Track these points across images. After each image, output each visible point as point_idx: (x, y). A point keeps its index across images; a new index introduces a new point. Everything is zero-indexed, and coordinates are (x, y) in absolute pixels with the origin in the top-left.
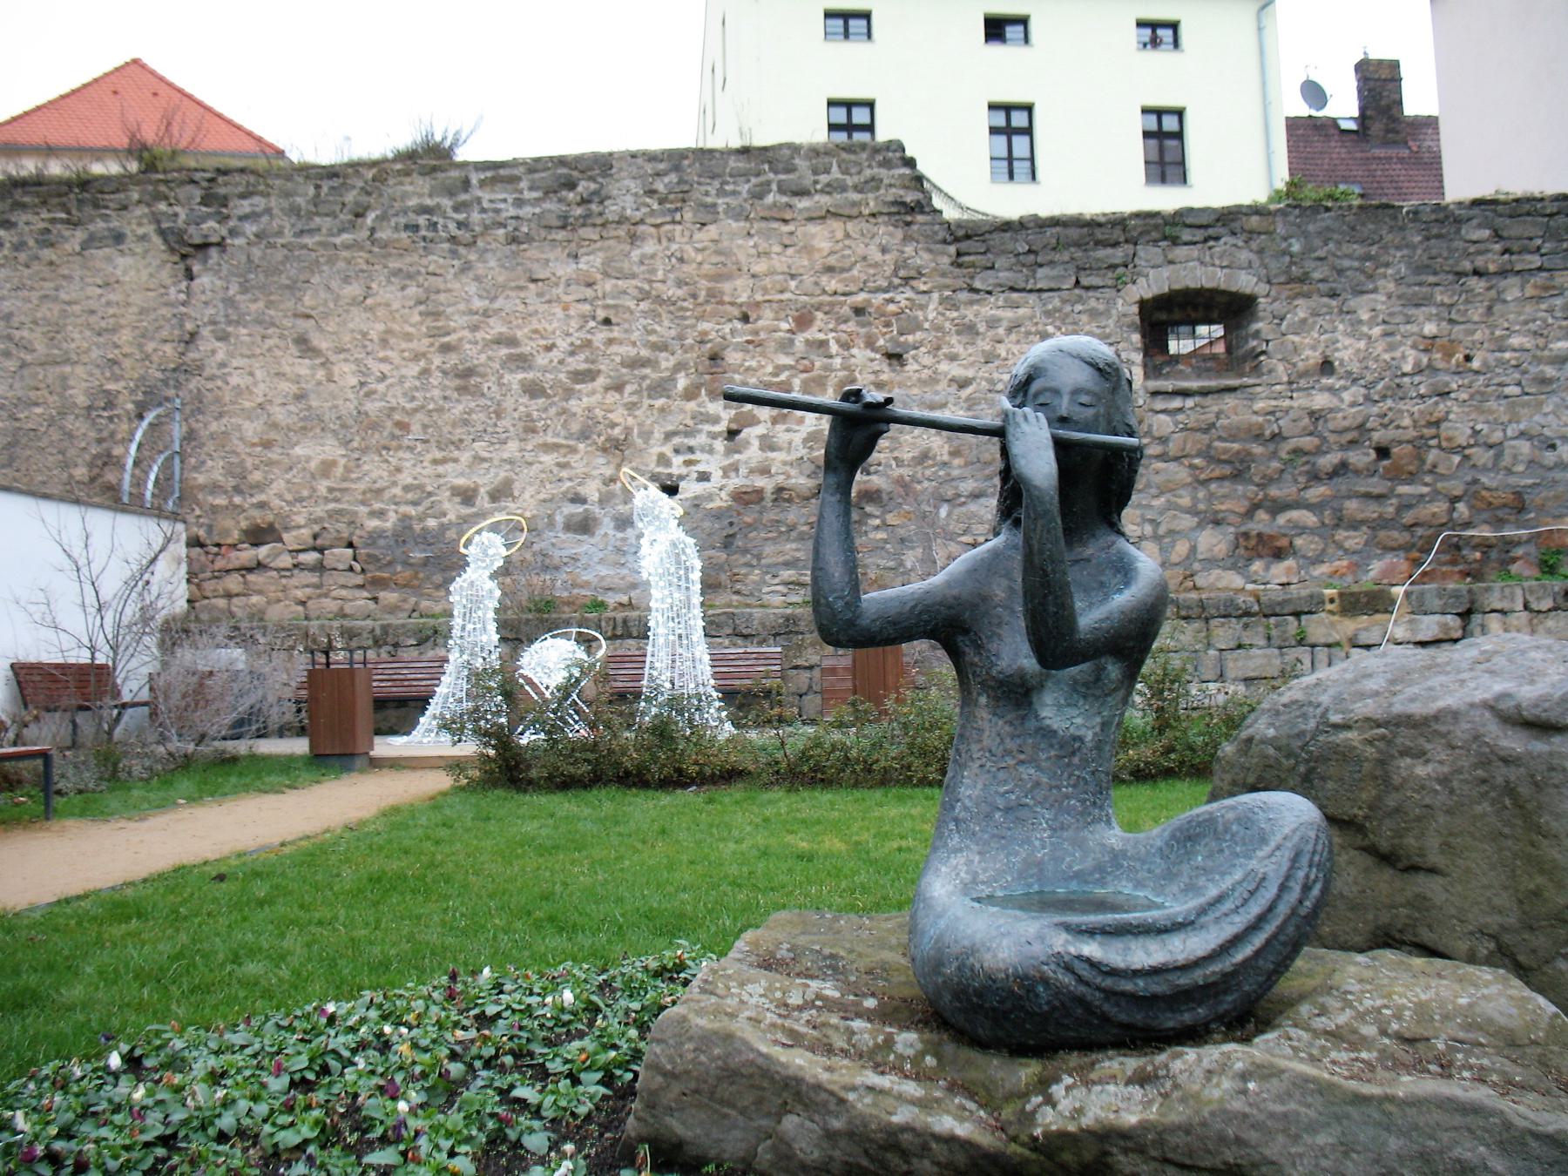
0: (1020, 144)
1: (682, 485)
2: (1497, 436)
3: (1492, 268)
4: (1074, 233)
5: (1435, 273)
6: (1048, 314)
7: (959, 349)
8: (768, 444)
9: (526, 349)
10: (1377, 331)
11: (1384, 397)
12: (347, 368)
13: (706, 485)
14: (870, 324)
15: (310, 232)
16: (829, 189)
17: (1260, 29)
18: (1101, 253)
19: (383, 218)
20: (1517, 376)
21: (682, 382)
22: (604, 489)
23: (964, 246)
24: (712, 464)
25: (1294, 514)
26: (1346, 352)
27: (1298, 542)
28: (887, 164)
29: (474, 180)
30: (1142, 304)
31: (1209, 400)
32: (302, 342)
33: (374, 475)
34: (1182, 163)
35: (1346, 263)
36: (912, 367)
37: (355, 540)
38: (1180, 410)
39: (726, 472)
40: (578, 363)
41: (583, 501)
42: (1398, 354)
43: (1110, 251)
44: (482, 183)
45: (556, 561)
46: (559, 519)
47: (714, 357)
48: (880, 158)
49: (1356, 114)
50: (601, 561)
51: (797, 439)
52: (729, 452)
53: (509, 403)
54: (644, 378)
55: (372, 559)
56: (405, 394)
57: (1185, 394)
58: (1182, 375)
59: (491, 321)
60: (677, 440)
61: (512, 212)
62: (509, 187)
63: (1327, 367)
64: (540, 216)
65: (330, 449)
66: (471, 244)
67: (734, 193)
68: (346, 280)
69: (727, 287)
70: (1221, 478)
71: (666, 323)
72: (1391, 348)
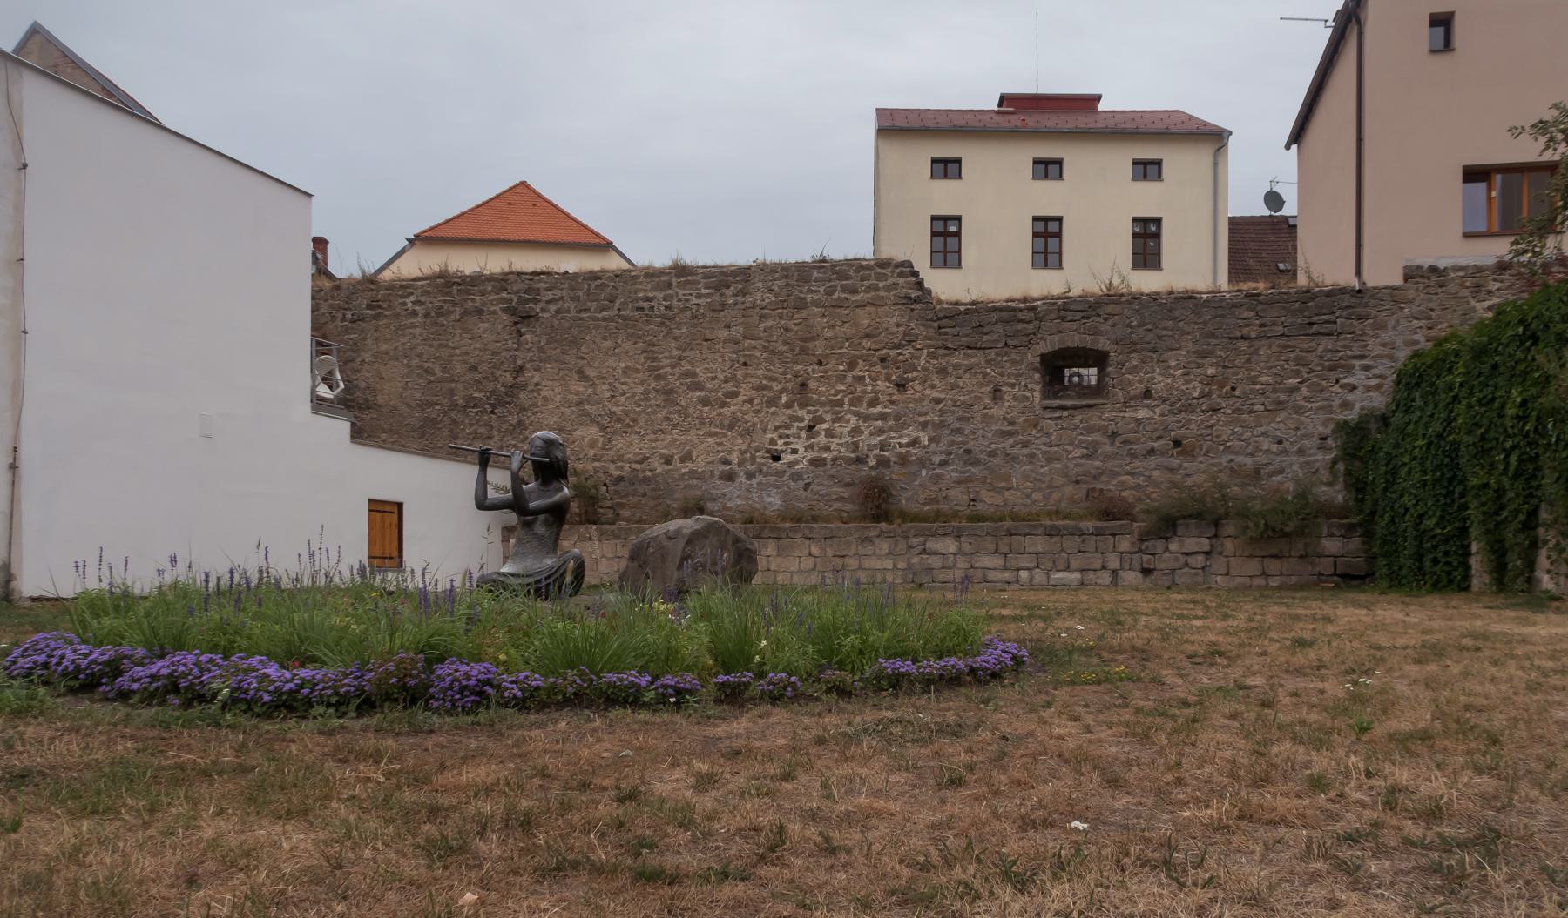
0: (1052, 242)
4: (1005, 315)
6: (988, 362)
7: (937, 382)
8: (830, 434)
10: (1179, 372)
11: (1180, 412)
12: (605, 387)
15: (585, 310)
17: (1216, 164)
18: (1020, 326)
21: (784, 399)
26: (1160, 384)
28: (901, 275)
29: (674, 281)
30: (1042, 356)
32: (580, 372)
34: (1158, 254)
38: (1060, 418)
39: (808, 448)
40: (729, 387)
51: (846, 431)
52: (808, 438)
53: (691, 410)
55: (617, 492)
58: (1069, 397)
63: (1147, 394)
66: (672, 319)
68: (604, 338)
69: (811, 345)
72: (1187, 382)
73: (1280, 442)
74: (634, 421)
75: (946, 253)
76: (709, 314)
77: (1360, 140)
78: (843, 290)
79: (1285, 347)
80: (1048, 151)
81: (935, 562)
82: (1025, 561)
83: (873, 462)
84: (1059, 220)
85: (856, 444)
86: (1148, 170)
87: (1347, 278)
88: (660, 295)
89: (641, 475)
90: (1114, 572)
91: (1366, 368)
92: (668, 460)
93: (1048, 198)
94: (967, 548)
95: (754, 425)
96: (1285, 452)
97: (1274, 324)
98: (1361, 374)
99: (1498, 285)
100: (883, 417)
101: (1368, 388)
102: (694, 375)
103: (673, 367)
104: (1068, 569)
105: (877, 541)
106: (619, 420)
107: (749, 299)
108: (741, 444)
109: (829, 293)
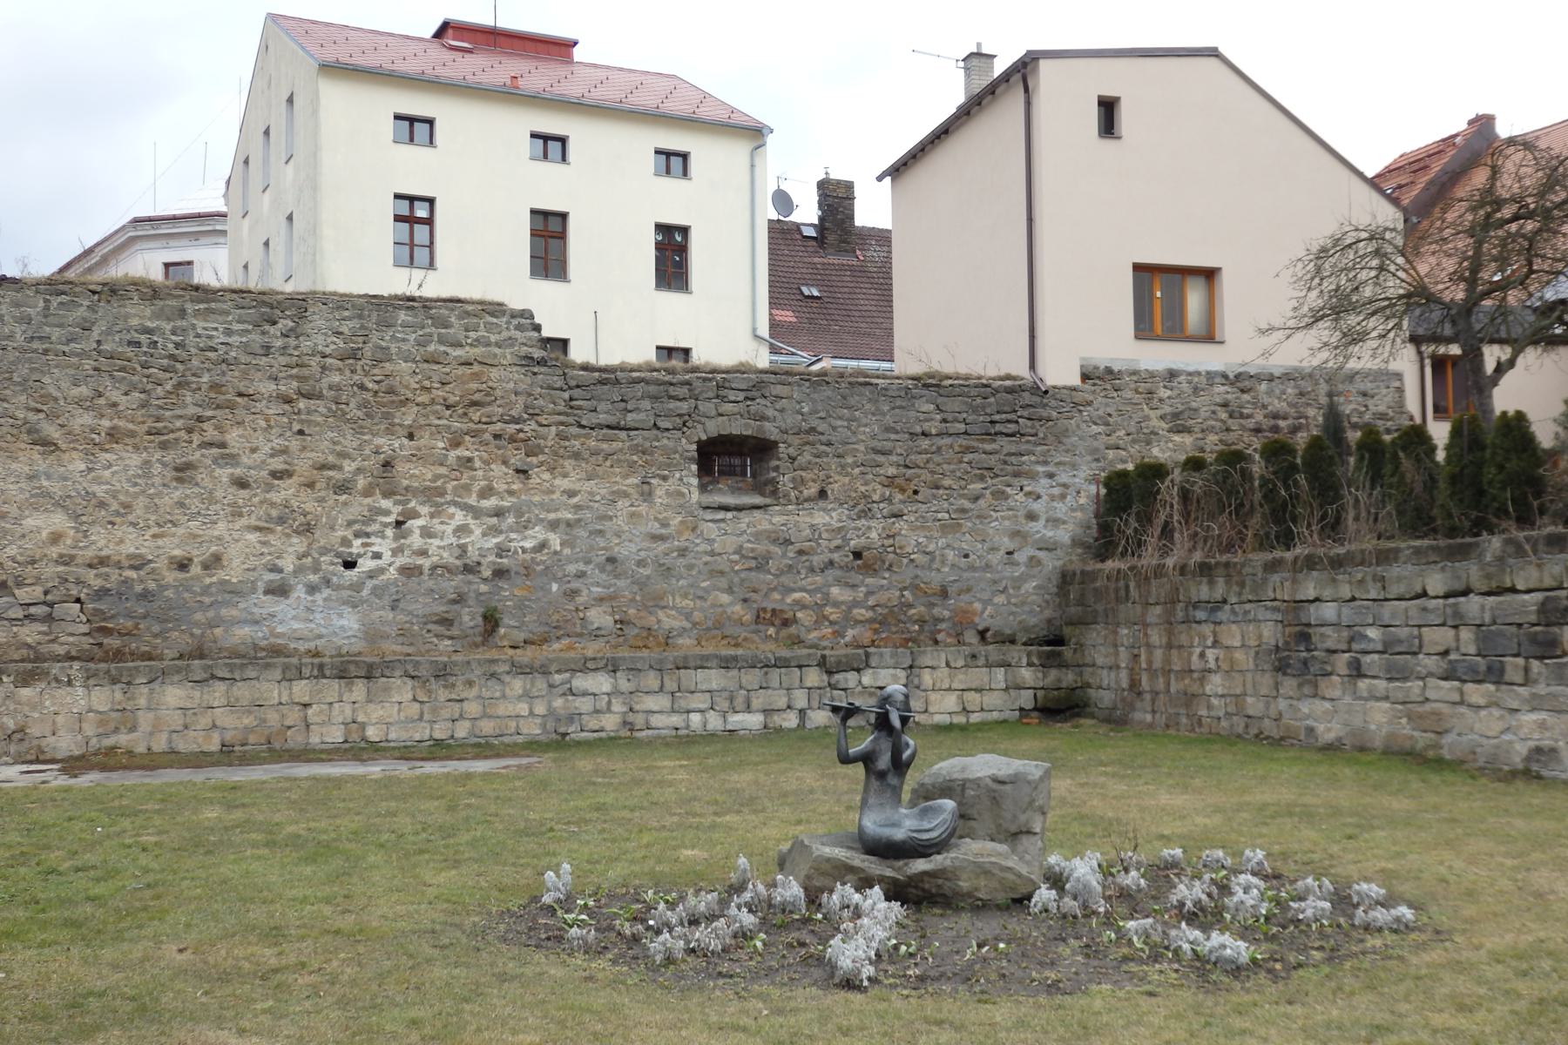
1: (360, 561)
2: (931, 548)
3: (934, 431)
4: (652, 389)
5: (897, 432)
8: (427, 533)
9: (235, 451)
10: (857, 471)
13: (379, 562)
14: (504, 447)
16: (477, 342)
18: (673, 405)
19: (109, 332)
20: (946, 505)
21: (361, 482)
22: (298, 563)
23: (577, 393)
24: (384, 546)
25: (797, 595)
27: (799, 615)
28: (519, 327)
31: (741, 515)
33: (101, 543)
35: (839, 423)
36: (534, 480)
37: (82, 596)
38: (723, 520)
39: (395, 552)
40: (277, 464)
41: (281, 571)
42: (869, 488)
43: (679, 404)
44: (197, 313)
45: (257, 617)
46: (261, 586)
47: (387, 464)
48: (515, 322)
49: (816, 222)
50: (294, 618)
51: (449, 529)
52: (396, 538)
53: (219, 494)
54: (330, 478)
56: (129, 480)
57: (726, 508)
59: (205, 426)
60: (356, 527)
61: (223, 339)
62: (220, 319)
64: (246, 345)
65: (59, 521)
67: (404, 340)
70: (750, 569)
71: (349, 437)
73: (966, 556)
74: (127, 506)
75: (412, 245)
76: (244, 358)
77: (1030, 220)
78: (441, 342)
79: (968, 448)
80: (552, 124)
81: (585, 705)
82: (699, 701)
83: (487, 573)
84: (563, 216)
85: (463, 549)
86: (673, 162)
87: (1021, 369)
88: (168, 327)
89: (138, 588)
90: (802, 712)
91: (1051, 476)
92: (183, 566)
93: (551, 187)
94: (624, 685)
95: (318, 518)
96: (972, 568)
97: (956, 420)
98: (1044, 481)
99: (1169, 393)
100: (499, 513)
101: (1052, 498)
102: (223, 445)
103: (190, 431)
104: (748, 709)
105: (507, 679)
106: (102, 505)
107: (306, 345)
108: (298, 544)
109: (420, 344)
